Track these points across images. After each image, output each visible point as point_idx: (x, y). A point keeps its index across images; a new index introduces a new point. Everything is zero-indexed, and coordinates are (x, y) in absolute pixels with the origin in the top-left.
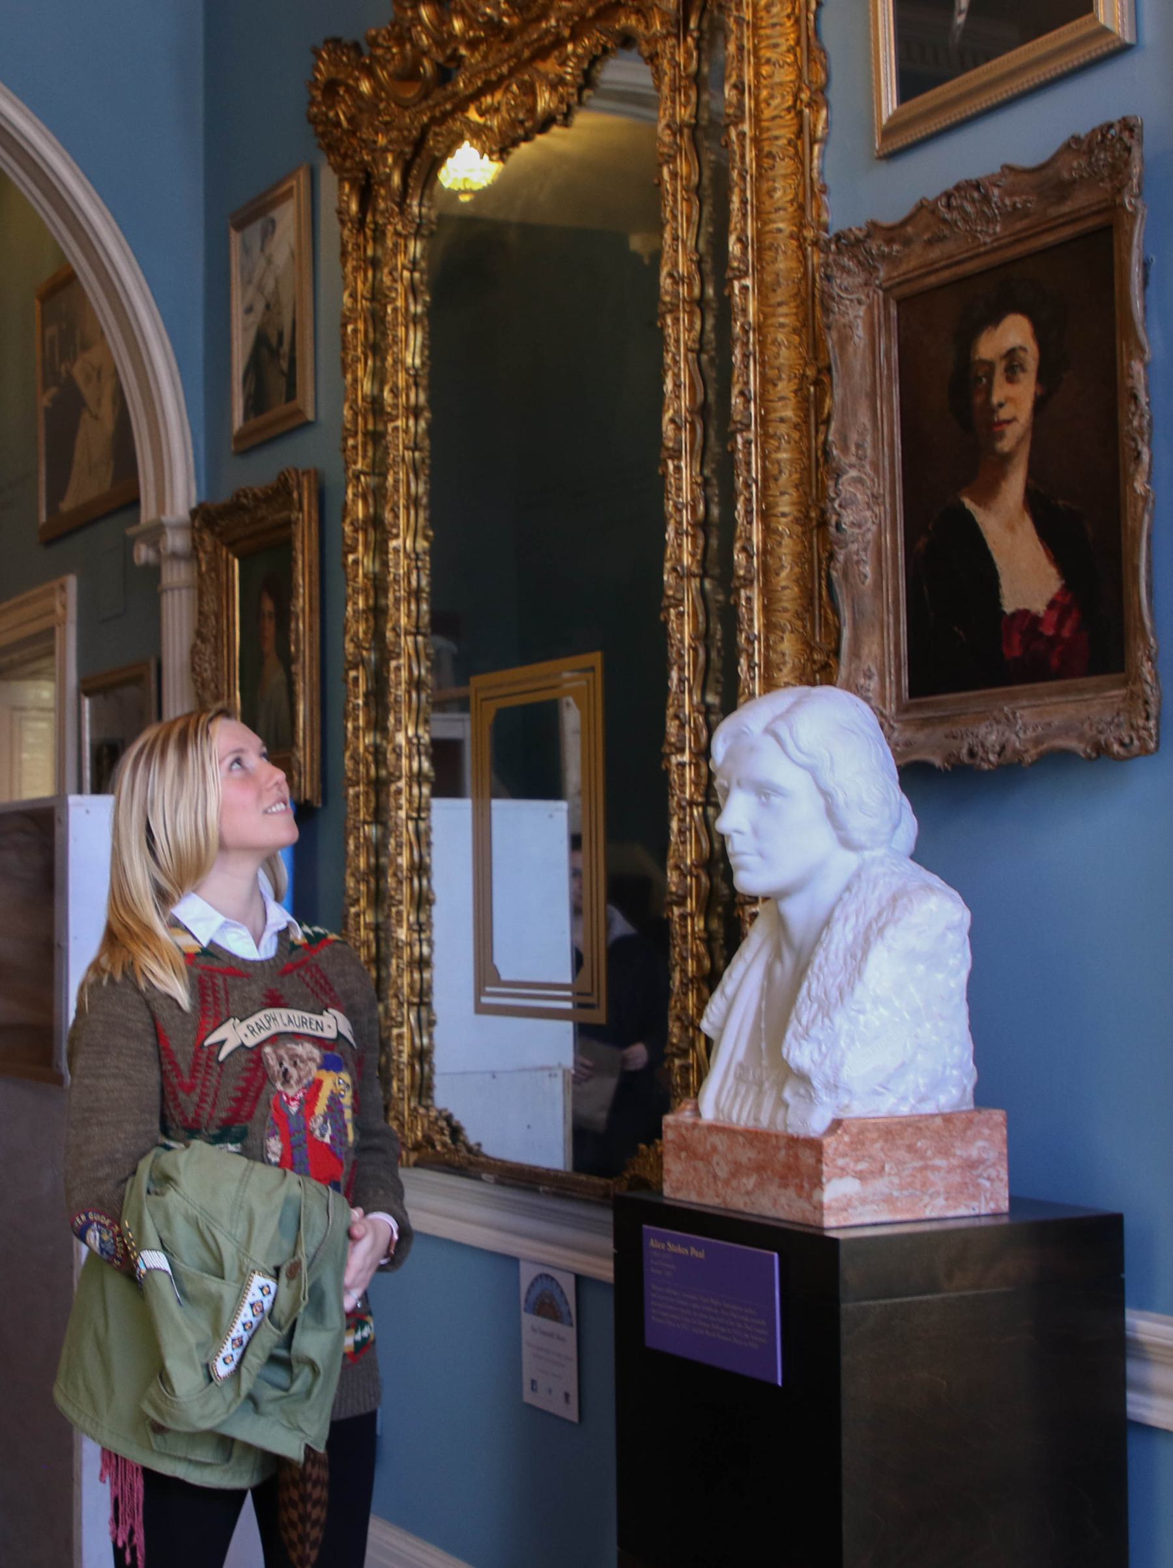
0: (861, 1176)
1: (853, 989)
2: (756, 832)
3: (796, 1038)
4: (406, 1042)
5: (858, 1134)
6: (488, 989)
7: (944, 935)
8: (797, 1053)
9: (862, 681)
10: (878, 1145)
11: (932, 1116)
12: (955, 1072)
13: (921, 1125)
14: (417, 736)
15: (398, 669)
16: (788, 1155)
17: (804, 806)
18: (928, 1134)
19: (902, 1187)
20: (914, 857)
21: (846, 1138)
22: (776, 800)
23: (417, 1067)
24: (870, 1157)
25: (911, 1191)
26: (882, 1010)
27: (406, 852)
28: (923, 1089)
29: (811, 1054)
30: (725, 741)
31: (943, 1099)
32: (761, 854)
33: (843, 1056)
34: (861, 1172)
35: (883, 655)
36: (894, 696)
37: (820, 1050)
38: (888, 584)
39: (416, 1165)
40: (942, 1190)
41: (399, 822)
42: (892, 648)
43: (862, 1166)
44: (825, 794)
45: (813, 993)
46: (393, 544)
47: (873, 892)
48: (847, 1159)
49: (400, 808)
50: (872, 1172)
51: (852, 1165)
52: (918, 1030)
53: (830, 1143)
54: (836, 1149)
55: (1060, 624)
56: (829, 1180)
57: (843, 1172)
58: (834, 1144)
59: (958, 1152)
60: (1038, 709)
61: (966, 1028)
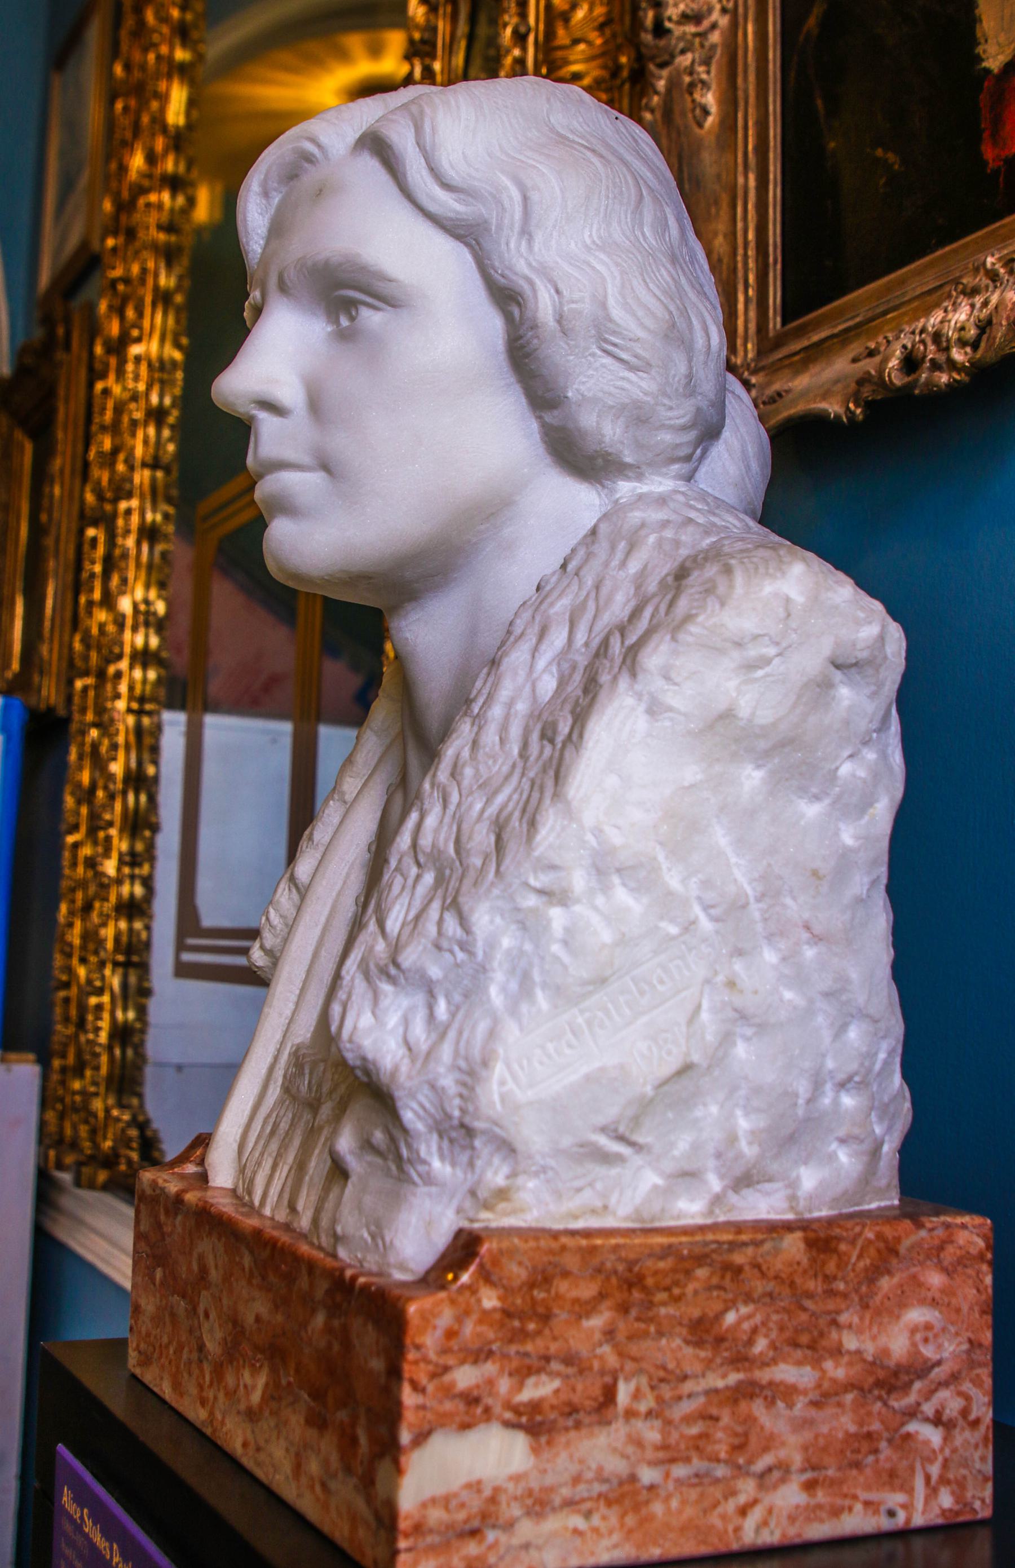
0: (535, 1424)
1: (533, 825)
2: (316, 405)
4: (106, 1016)
5: (532, 1285)
6: (191, 941)
7: (824, 686)
8: (366, 1020)
10: (596, 1322)
11: (776, 1229)
12: (848, 1101)
13: (739, 1258)
14: (147, 602)
15: (128, 512)
16: (328, 1329)
17: (448, 327)
18: (760, 1286)
19: (669, 1455)
20: (762, 521)
21: (490, 1300)
22: (372, 318)
23: (118, 1052)
24: (569, 1360)
25: (698, 1464)
26: (622, 895)
27: (121, 755)
28: (748, 1150)
29: (406, 1022)
30: (266, 194)
31: (809, 1179)
32: (325, 466)
33: (492, 1034)
34: (535, 1407)
35: (734, 253)
36: (752, 327)
37: (431, 1016)
38: (748, 117)
39: (105, 1188)
40: (797, 1460)
41: (116, 716)
42: (751, 236)
43: (540, 1389)
44: (506, 297)
45: (426, 841)
46: (135, 350)
47: (623, 564)
48: (490, 1368)
49: (117, 696)
50: (571, 1409)
51: (504, 1385)
52: (738, 966)
53: (431, 1323)
54: (451, 1334)
56: (421, 1438)
57: (472, 1411)
58: (446, 1318)
59: (851, 1342)
61: (884, 972)
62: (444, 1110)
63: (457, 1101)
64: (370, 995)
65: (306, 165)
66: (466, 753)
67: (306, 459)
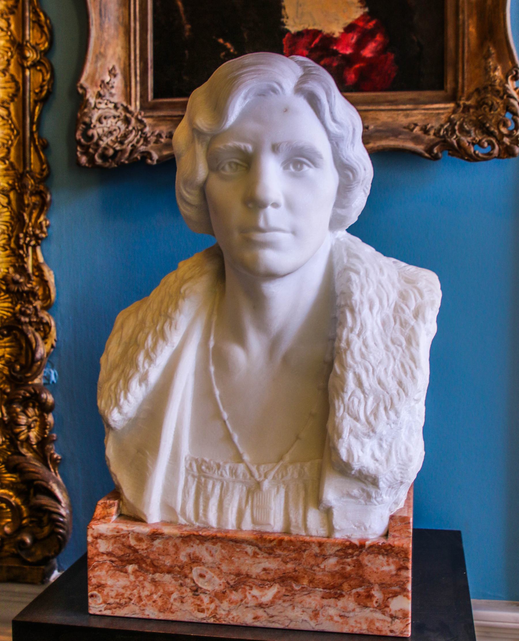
3: (357, 437)
9: (107, 79)
30: (245, 98)
32: (294, 232)
33: (407, 449)
55: (360, 45)
60: (405, 112)
62: (395, 479)
63: (400, 475)
64: (359, 443)
65: (272, 93)
66: (363, 349)
67: (287, 228)
